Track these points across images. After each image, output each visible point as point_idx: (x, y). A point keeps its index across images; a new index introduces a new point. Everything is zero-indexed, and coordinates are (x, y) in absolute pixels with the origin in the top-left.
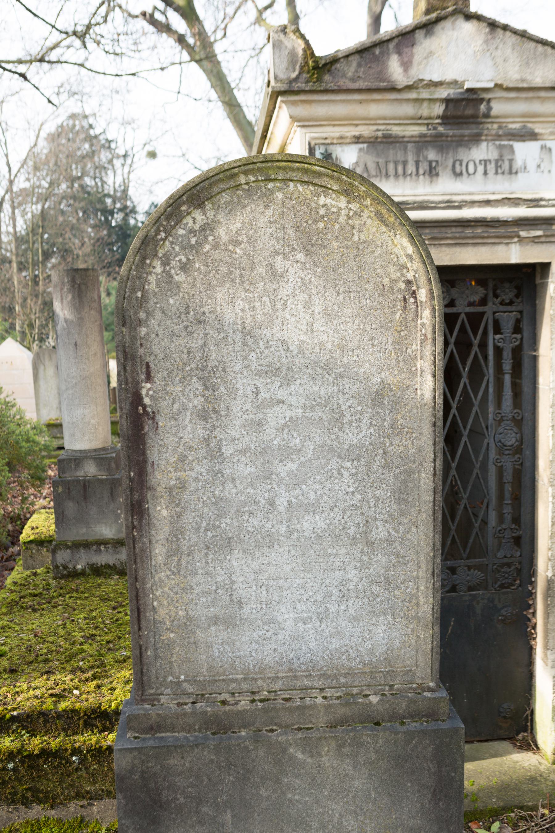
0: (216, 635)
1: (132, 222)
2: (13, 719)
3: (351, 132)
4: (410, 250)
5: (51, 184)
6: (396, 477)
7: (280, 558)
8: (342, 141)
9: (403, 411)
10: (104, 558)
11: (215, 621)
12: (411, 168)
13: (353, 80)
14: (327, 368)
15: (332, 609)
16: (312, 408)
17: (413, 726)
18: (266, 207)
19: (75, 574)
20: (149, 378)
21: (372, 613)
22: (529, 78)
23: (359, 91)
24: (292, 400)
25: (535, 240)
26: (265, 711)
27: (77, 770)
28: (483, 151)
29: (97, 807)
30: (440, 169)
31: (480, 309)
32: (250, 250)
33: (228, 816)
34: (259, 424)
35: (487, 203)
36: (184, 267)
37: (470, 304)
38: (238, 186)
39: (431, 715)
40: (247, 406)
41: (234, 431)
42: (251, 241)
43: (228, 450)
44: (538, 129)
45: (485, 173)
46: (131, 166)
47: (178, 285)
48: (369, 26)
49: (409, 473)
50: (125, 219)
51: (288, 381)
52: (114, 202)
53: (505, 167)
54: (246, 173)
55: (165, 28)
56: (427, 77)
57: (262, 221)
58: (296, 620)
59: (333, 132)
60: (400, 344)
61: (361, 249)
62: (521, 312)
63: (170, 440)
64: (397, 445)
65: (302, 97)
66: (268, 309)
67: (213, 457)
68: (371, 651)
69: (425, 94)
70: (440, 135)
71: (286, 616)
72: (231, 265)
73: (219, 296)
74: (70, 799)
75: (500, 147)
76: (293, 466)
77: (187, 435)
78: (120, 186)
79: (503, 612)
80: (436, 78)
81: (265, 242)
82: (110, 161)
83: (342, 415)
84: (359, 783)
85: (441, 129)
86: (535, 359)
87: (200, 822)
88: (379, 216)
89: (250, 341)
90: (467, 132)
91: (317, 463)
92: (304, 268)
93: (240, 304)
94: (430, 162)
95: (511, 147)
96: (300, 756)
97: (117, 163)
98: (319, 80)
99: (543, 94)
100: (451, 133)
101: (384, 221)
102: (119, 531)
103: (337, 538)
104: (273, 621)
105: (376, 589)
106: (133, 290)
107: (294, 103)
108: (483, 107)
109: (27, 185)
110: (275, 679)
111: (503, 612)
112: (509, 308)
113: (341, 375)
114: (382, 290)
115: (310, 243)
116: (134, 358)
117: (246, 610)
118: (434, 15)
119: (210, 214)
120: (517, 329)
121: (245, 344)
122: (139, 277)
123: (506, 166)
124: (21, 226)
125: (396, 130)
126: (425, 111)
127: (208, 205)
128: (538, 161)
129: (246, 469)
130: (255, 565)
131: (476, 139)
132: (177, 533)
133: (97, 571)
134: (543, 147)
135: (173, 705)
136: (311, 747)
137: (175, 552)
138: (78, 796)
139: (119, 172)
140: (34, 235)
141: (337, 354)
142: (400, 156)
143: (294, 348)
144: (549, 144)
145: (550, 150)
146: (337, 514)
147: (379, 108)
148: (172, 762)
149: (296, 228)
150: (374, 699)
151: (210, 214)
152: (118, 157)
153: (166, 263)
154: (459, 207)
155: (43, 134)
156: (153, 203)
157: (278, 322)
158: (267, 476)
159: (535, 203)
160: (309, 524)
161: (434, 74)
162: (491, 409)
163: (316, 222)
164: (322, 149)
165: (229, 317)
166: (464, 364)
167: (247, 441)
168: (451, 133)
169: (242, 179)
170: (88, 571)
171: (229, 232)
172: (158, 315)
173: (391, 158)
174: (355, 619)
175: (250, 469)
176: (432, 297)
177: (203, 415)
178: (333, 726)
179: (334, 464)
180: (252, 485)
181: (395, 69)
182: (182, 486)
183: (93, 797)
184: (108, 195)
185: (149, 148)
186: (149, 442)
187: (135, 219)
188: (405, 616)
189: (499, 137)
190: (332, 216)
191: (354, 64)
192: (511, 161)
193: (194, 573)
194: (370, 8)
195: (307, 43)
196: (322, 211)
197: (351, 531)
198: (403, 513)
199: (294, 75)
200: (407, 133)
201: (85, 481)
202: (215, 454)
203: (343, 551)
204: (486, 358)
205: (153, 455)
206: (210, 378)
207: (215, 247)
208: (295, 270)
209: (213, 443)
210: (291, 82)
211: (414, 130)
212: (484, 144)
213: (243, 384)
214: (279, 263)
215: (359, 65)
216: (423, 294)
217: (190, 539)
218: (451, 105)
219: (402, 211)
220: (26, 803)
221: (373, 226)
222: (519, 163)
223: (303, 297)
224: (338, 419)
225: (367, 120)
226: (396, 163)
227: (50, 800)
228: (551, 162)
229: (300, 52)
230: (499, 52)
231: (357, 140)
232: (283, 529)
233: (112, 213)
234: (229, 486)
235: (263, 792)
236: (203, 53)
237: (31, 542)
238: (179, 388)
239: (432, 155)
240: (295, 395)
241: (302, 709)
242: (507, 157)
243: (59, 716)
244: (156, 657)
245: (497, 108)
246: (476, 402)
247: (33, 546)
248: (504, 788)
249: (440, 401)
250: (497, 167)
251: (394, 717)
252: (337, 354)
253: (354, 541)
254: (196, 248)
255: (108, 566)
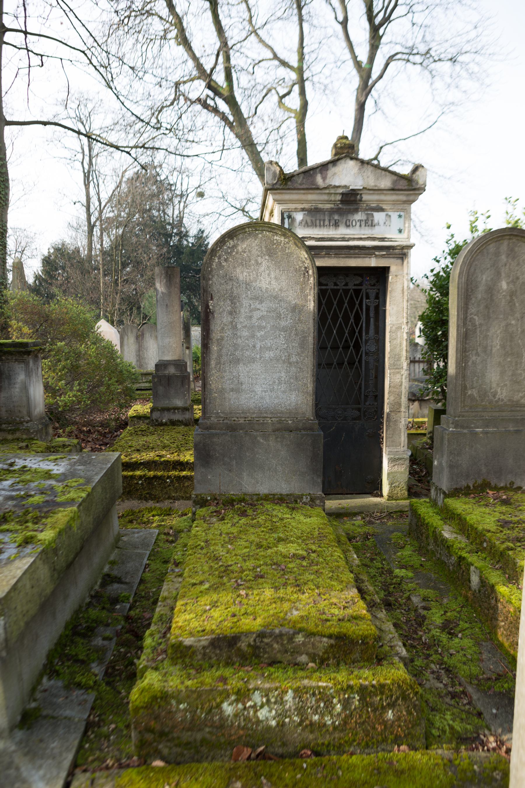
0: (232, 396)
1: (185, 243)
2: (141, 464)
3: (302, 206)
4: (306, 256)
5: (129, 214)
6: (300, 339)
7: (257, 367)
8: (296, 210)
9: (303, 314)
10: (177, 417)
11: (232, 390)
12: (327, 223)
13: (301, 184)
14: (276, 297)
15: (275, 388)
16: (270, 312)
17: (303, 432)
18: (255, 240)
19: (162, 424)
20: (212, 299)
21: (290, 390)
22: (378, 185)
23: (303, 189)
24: (263, 309)
25: (383, 256)
26: (249, 424)
27: (169, 486)
28: (359, 216)
29: (177, 503)
30: (340, 223)
31: (360, 287)
32: (249, 254)
33: (234, 462)
34: (251, 317)
35: (361, 239)
36: (226, 260)
37: (355, 285)
38: (246, 232)
39: (311, 429)
40: (247, 310)
41: (242, 319)
42: (250, 251)
43: (239, 326)
44: (384, 207)
45: (360, 226)
46: (185, 202)
47: (223, 266)
48: (356, 110)
49: (305, 337)
50: (180, 241)
51: (261, 302)
52: (173, 228)
53: (370, 223)
54: (248, 228)
55: (215, 110)
56: (333, 183)
57: (254, 245)
58: (262, 391)
59: (292, 206)
60: (302, 290)
61: (289, 255)
62: (379, 290)
63: (219, 322)
64: (300, 327)
65: (279, 191)
66: (255, 276)
67: (234, 329)
68: (290, 405)
69: (332, 191)
70: (340, 209)
71: (258, 389)
72: (242, 260)
73: (238, 270)
74: (165, 499)
75: (367, 214)
76: (263, 333)
77: (225, 320)
78: (177, 217)
79: (368, 431)
80: (337, 184)
81: (255, 252)
82: (171, 200)
83: (281, 315)
84: (283, 453)
85: (340, 206)
86: (385, 311)
87: (224, 464)
88: (295, 244)
89: (248, 287)
90: (352, 207)
91: (271, 332)
92: (268, 262)
93: (245, 274)
94: (336, 220)
95: (372, 214)
96: (262, 441)
97: (176, 200)
98: (286, 184)
99: (385, 192)
100: (345, 207)
101: (297, 246)
102: (186, 403)
103: (278, 360)
104: (254, 391)
105: (292, 381)
106: (208, 268)
107: (275, 194)
108: (358, 197)
109: (111, 215)
110: (254, 413)
111: (368, 431)
112: (373, 287)
113: (281, 300)
114: (296, 270)
115: (271, 253)
116: (207, 292)
117: (244, 386)
118: (337, 157)
119: (236, 242)
120: (377, 297)
121: (246, 288)
122: (210, 263)
123: (370, 222)
124: (107, 243)
125: (320, 206)
126: (333, 198)
127: (235, 239)
128: (384, 221)
129: (245, 333)
130: (247, 369)
131: (356, 211)
132: (220, 356)
133: (173, 423)
134: (387, 215)
135: (216, 420)
136: (266, 437)
137: (218, 363)
138: (169, 498)
139: (177, 207)
140: (116, 250)
141: (279, 293)
142: (322, 218)
143: (264, 290)
144: (390, 213)
145: (390, 216)
146: (278, 352)
147: (312, 197)
148: (215, 440)
149: (266, 247)
150: (290, 422)
151: (236, 242)
152: (177, 196)
153: (219, 258)
154: (348, 241)
155: (124, 179)
156: (200, 230)
157: (258, 280)
158: (253, 336)
159: (383, 239)
160: (268, 355)
161: (336, 182)
162: (364, 334)
163: (273, 245)
164: (287, 214)
165: (241, 278)
166: (352, 313)
167: (246, 323)
168: (345, 207)
169: (247, 230)
170: (168, 423)
171: (242, 248)
172: (216, 277)
173: (318, 218)
174: (284, 392)
175: (247, 334)
176: (314, 273)
177: (231, 313)
178: (274, 431)
179: (277, 333)
180: (247, 339)
181: (319, 180)
182: (222, 338)
183: (175, 499)
184: (169, 224)
185: (199, 190)
186: (211, 322)
187: (187, 240)
188: (303, 392)
189: (366, 210)
190: (279, 243)
191: (301, 178)
192: (372, 221)
193: (225, 372)
194: (357, 99)
195: (281, 168)
196: (275, 242)
197: (283, 358)
198: (302, 352)
199: (275, 182)
200: (325, 207)
201: (169, 376)
202: (235, 328)
203: (280, 366)
204: (362, 310)
205: (212, 327)
206: (234, 299)
207: (237, 253)
208: (265, 262)
209: (234, 323)
210: (273, 185)
211: (328, 206)
212: (360, 213)
213: (245, 302)
214: (259, 260)
215: (303, 178)
216: (311, 272)
217: (224, 359)
218: (344, 196)
219: (303, 242)
220: (146, 500)
221: (293, 247)
222: (376, 221)
223: (267, 272)
224: (279, 317)
225: (307, 201)
226: (320, 220)
227: (157, 499)
228: (390, 221)
229: (278, 172)
230: (365, 174)
231: (303, 210)
232: (258, 356)
233: (170, 236)
234: (239, 339)
235: (248, 454)
236: (238, 124)
237: (134, 417)
238: (222, 303)
239: (336, 217)
240: (264, 307)
241: (263, 424)
242: (370, 219)
243: (162, 463)
244: (210, 403)
245: (365, 197)
246: (357, 331)
247: (135, 419)
248: (362, 506)
249: (316, 311)
250: (366, 223)
251: (297, 429)
252: (279, 293)
253: (284, 362)
254: (230, 254)
255: (179, 421)
